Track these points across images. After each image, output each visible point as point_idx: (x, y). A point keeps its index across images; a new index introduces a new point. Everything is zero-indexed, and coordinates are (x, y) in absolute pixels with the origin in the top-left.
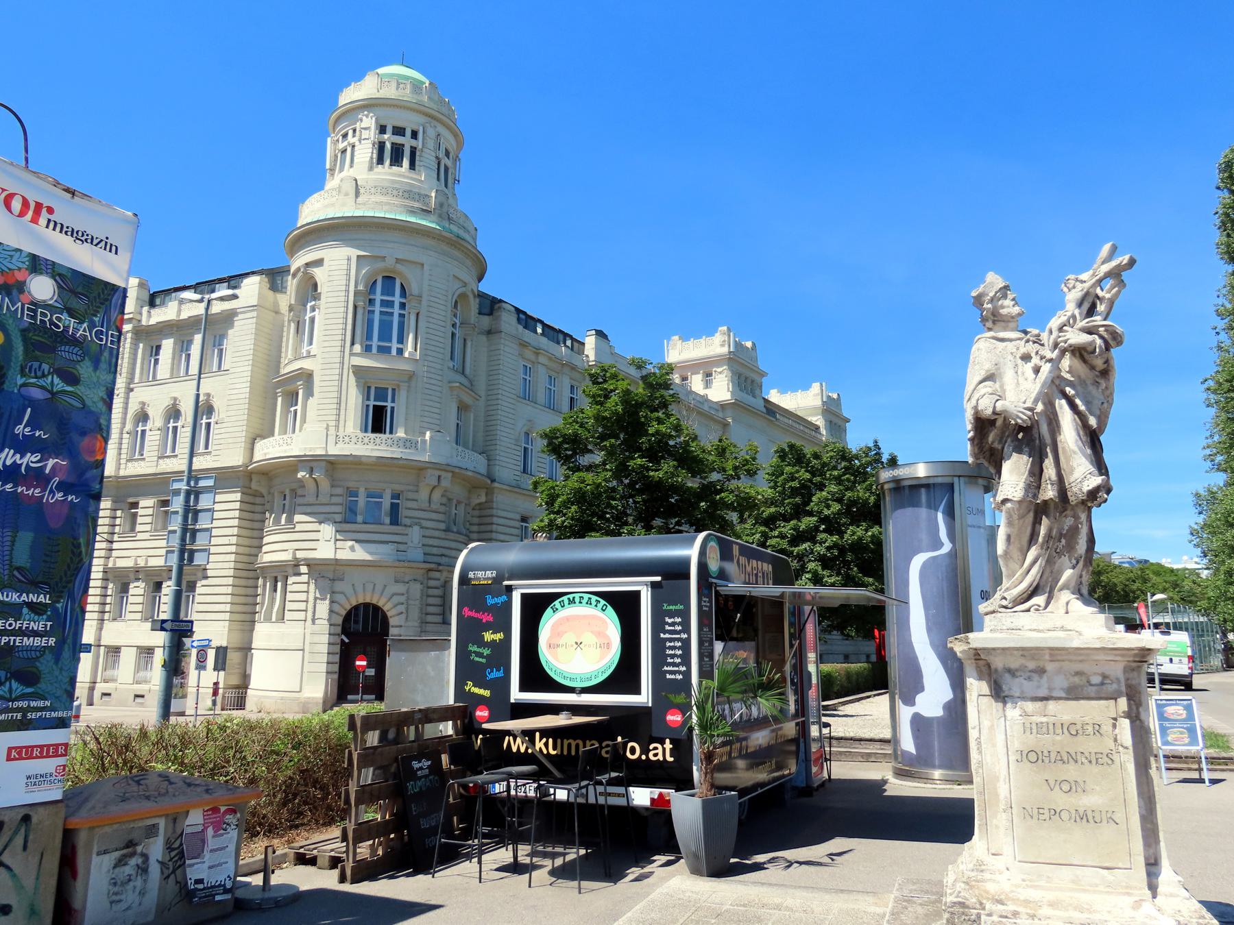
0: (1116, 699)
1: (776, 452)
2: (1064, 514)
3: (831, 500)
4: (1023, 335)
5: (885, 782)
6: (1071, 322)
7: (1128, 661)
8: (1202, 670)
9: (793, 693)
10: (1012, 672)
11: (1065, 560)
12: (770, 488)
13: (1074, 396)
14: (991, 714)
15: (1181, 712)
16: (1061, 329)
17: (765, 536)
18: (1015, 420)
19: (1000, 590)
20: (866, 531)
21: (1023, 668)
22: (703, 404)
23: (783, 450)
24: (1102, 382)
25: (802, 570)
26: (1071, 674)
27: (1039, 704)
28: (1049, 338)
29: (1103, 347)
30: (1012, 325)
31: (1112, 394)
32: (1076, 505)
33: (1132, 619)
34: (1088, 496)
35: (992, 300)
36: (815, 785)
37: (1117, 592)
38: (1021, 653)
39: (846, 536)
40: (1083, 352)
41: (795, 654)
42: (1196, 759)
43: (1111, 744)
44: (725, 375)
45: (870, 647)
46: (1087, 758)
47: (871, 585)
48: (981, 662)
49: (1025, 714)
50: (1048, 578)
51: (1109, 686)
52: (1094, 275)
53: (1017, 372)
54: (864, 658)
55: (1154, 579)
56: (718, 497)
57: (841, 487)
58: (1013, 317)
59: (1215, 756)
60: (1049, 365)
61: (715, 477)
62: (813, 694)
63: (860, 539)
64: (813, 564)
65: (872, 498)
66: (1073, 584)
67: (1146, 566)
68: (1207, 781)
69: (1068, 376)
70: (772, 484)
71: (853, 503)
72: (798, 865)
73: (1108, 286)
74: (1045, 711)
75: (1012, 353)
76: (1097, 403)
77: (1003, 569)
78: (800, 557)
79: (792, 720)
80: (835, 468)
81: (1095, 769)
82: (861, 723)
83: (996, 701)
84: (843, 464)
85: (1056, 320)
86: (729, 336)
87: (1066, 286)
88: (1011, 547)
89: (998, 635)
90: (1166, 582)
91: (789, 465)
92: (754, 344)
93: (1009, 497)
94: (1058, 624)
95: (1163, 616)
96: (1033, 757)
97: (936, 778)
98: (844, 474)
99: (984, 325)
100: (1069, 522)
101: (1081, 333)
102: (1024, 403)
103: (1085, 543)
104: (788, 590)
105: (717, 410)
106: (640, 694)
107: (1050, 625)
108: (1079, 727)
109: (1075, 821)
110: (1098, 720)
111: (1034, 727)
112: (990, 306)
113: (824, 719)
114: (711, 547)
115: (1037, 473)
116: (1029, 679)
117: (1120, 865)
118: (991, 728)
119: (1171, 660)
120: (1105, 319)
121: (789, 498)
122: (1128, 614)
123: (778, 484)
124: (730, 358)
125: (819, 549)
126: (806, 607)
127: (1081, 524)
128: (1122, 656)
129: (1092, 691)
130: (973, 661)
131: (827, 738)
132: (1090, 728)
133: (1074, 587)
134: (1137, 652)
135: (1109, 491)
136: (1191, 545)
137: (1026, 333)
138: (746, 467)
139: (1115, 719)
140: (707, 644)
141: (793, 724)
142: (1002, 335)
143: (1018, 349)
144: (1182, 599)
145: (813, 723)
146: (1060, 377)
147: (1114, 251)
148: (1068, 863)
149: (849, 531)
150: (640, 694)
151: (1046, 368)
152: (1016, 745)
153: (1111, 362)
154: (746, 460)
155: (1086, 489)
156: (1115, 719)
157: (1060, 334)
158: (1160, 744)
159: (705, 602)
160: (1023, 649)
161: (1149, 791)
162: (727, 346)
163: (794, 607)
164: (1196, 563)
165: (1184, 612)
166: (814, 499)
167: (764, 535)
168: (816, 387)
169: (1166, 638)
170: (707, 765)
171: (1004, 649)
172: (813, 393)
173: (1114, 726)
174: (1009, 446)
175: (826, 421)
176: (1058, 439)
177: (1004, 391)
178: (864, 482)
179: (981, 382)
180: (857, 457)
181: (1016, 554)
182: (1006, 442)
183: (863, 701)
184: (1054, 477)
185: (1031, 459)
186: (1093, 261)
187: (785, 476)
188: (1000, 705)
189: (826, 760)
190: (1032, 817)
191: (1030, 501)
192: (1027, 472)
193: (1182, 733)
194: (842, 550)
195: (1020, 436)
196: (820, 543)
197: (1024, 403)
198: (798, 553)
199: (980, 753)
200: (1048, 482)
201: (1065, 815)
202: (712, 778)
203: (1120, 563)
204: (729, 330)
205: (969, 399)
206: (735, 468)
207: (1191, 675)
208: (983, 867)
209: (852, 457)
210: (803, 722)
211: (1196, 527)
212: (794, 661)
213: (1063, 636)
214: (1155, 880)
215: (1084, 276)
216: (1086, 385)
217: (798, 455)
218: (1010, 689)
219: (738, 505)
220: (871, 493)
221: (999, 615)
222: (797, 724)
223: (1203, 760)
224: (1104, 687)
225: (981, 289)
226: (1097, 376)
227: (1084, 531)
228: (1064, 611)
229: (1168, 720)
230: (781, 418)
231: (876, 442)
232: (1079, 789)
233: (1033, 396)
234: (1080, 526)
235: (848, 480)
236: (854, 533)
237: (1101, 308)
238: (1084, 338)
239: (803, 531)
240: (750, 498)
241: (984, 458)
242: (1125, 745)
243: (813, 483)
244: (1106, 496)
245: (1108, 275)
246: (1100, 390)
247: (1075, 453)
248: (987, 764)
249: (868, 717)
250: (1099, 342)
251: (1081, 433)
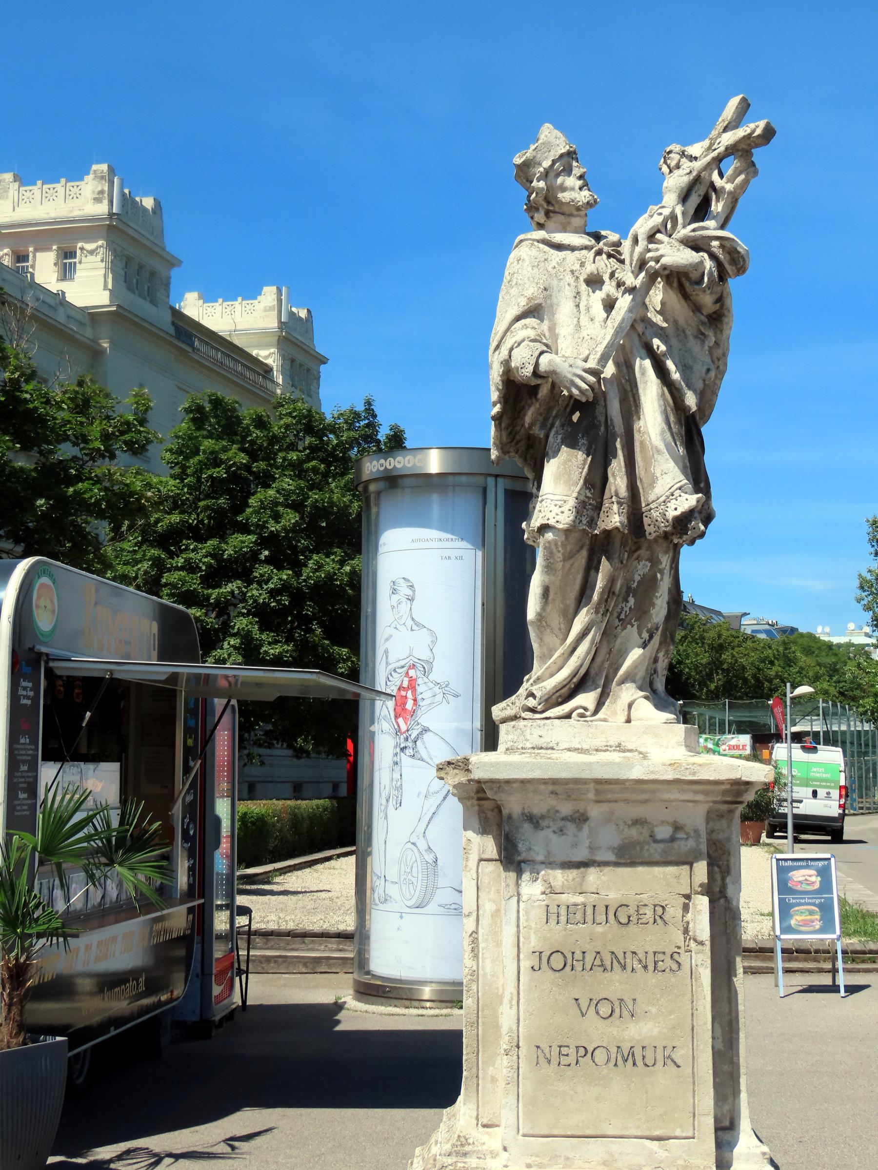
0: (691, 865)
1: (188, 411)
2: (636, 555)
3: (281, 504)
4: (593, 241)
5: (338, 1007)
6: (669, 226)
7: (715, 802)
8: (862, 808)
9: (186, 854)
10: (534, 820)
11: (632, 632)
12: (173, 477)
13: (664, 355)
14: (498, 892)
15: (813, 879)
16: (651, 238)
17: (159, 565)
18: (569, 391)
19: (528, 680)
20: (342, 563)
21: (552, 814)
22: (55, 309)
23: (200, 409)
24: (710, 333)
25: (225, 630)
26: (625, 823)
27: (573, 874)
28: (632, 252)
29: (716, 274)
30: (576, 222)
31: (725, 355)
32: (656, 540)
33: (765, 725)
34: (674, 526)
35: (546, 175)
36: (217, 1018)
37: (746, 681)
38: (550, 788)
39: (306, 572)
40: (683, 279)
41: (193, 786)
42: (828, 953)
43: (679, 938)
44: (99, 258)
45: (338, 770)
46: (640, 961)
47: (345, 661)
48: (487, 804)
49: (551, 891)
50: (603, 663)
51: (683, 842)
52: (710, 149)
53: (578, 306)
54: (328, 789)
55: (803, 660)
56: (71, 489)
57: (302, 483)
58: (578, 209)
59: (859, 947)
60: (628, 298)
61: (66, 451)
62: (221, 861)
63: (330, 577)
64: (245, 621)
65: (356, 504)
66: (641, 674)
67: (792, 638)
68: (842, 989)
69: (658, 319)
70: (177, 470)
71: (321, 512)
72: (171, 1160)
73: (729, 172)
74: (581, 885)
75: (572, 272)
76: (699, 369)
77: (535, 646)
78: (223, 608)
79: (182, 903)
80: (292, 447)
81: (652, 979)
82: (310, 905)
83: (506, 869)
84: (308, 440)
85: (646, 220)
86: (111, 183)
87: (665, 162)
88: (549, 608)
89: (515, 758)
90: (819, 665)
91: (210, 436)
92: (157, 203)
93: (552, 522)
94: (613, 741)
95: (812, 721)
97: (426, 997)
98: (309, 459)
99: (532, 218)
100: (642, 568)
101: (682, 247)
102: (586, 360)
103: (665, 606)
104: (185, 669)
105: (82, 324)
107: (599, 742)
108: (632, 911)
109: (616, 1065)
110: (662, 897)
111: (563, 911)
112: (542, 184)
113: (241, 900)
114: (42, 585)
115: (598, 482)
116: (561, 831)
117: (678, 1133)
118: (496, 913)
119: (815, 794)
120: (722, 227)
121: (208, 497)
122: (759, 717)
123: (189, 471)
124: (110, 227)
125: (255, 592)
126: (216, 700)
127: (661, 572)
128: (706, 793)
129: (655, 850)
130: (475, 802)
131: (244, 933)
132: (649, 912)
133: (644, 679)
134: (728, 786)
135: (708, 519)
136: (859, 607)
137: (598, 237)
138: (127, 437)
139: (688, 897)
140: (26, 768)
141: (183, 908)
142: (559, 237)
143: (582, 265)
144: (841, 694)
145: (220, 908)
146: (646, 320)
147: (744, 107)
148: (599, 1133)
149: (311, 563)
151: (624, 302)
152: (532, 942)
153: (727, 302)
154: (127, 423)
155: (671, 514)
156: (688, 897)
157: (651, 246)
158: (778, 932)
159: (25, 688)
160: (554, 782)
161: (730, 1011)
162: (106, 202)
163: (197, 700)
164: (867, 635)
165: (842, 715)
166: (252, 501)
167: (158, 564)
168: (269, 294)
169: (811, 757)
170: (12, 990)
171: (523, 782)
172: (262, 305)
173: (686, 908)
174: (557, 433)
175: (284, 358)
176: (636, 427)
177: (555, 337)
178: (343, 475)
179: (518, 318)
180: (333, 429)
181: (556, 620)
182: (552, 426)
183: (319, 867)
184: (623, 492)
185: (590, 459)
186: (712, 126)
187: (201, 457)
188: (512, 875)
189: (240, 972)
190: (549, 1061)
191: (584, 530)
192: (582, 481)
193: (811, 913)
194: (298, 596)
195: (576, 417)
196: (260, 583)
197: (586, 360)
198: (217, 600)
199: (476, 957)
200: (614, 499)
201: (600, 1056)
202: (21, 1012)
203: (753, 631)
204: (112, 171)
205: (498, 347)
206: (106, 437)
207: (842, 817)
208: (467, 1148)
209: (324, 428)
210: (201, 907)
211: (868, 577)
212: (189, 798)
213: (617, 760)
214: (727, 1154)
215: (695, 149)
216: (686, 336)
217: (228, 418)
218: (530, 849)
219: (108, 506)
220: (354, 495)
221: (522, 723)
222: (190, 910)
223: (840, 955)
224: (676, 845)
225: (529, 154)
226: (703, 323)
227: (665, 584)
228: (624, 718)
229: (792, 891)
230: (203, 348)
231: (369, 403)
232: (625, 1013)
233: (600, 349)
234: (659, 575)
235: (315, 470)
236: (319, 567)
237: (717, 207)
238: (685, 257)
239: (230, 560)
240: (132, 494)
241: (517, 452)
242: (699, 939)
243: (250, 472)
244: (702, 527)
245: (732, 150)
246: (706, 348)
247: (659, 451)
248: (485, 975)
249: (323, 895)
250: (709, 264)
251: (672, 419)
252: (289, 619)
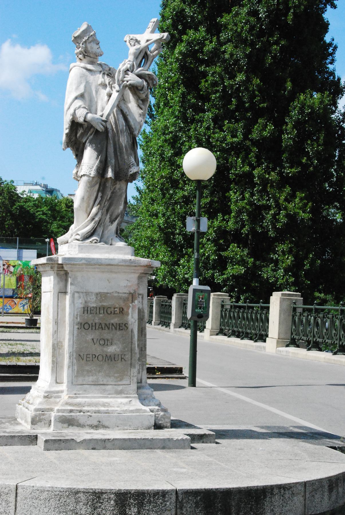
81: (119, 333)
106: (199, 285)
120: (147, 70)
150: (199, 285)
201: (100, 358)
252: (236, 290)
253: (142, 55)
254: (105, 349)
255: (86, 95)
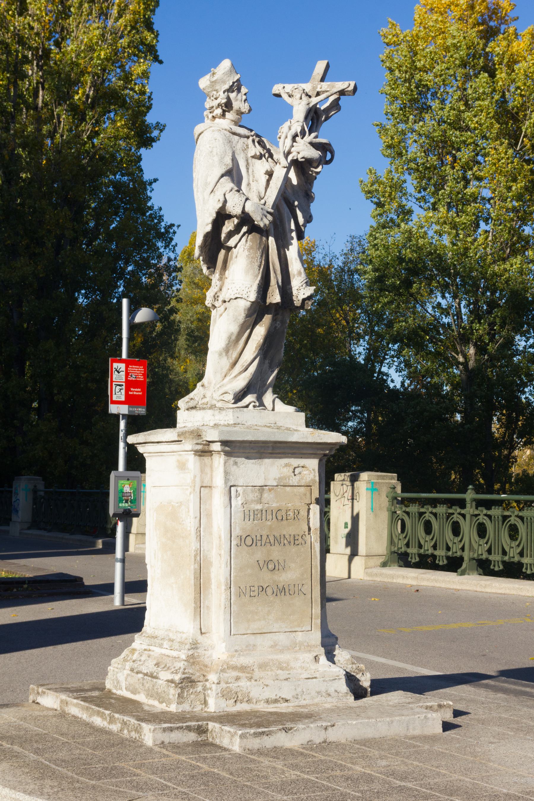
81: (294, 549)
96: (249, 541)
108: (284, 513)
152: (237, 532)
201: (269, 591)
253: (312, 114)
254: (276, 578)
255: (234, 172)
